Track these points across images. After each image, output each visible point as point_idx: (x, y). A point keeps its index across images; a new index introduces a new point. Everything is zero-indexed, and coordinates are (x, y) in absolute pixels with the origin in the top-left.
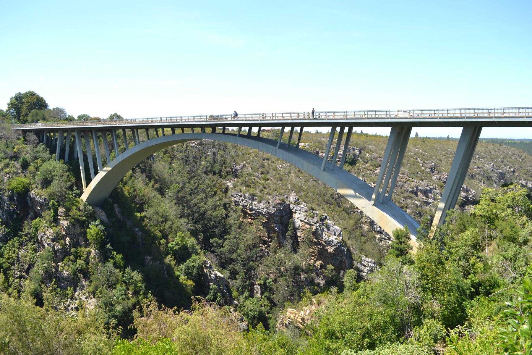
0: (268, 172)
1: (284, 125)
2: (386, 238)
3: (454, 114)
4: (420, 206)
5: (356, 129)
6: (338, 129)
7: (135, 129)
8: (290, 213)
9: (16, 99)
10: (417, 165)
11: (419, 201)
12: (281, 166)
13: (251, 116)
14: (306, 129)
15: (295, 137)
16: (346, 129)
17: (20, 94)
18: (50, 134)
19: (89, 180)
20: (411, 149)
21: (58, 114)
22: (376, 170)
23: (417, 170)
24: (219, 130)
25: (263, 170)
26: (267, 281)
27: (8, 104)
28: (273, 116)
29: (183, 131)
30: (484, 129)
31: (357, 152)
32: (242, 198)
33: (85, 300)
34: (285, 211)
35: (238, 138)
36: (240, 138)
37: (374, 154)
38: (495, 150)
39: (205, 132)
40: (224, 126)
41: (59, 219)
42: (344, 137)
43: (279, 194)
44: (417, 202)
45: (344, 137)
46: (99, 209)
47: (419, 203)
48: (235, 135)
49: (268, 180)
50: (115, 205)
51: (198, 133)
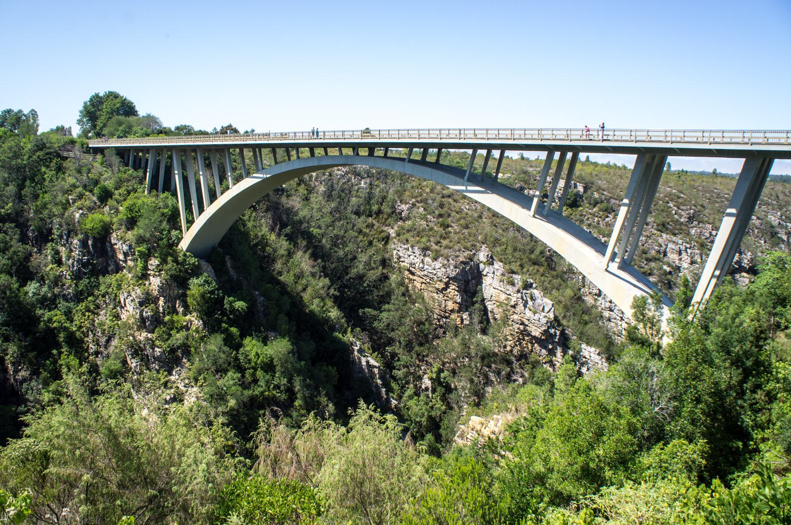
0: (449, 216)
1: (475, 147)
2: (618, 318)
3: (731, 138)
4: (670, 273)
5: (582, 156)
6: (557, 155)
7: (256, 148)
8: (478, 277)
9: (93, 105)
10: (667, 212)
11: (669, 265)
12: (467, 207)
13: (681, 134)
14: (508, 153)
15: (492, 165)
16: (569, 155)
17: (97, 96)
18: (138, 154)
19: (190, 222)
20: (663, 189)
21: (152, 126)
22: (607, 217)
23: (668, 220)
24: (379, 152)
25: (443, 211)
26: (442, 375)
27: (81, 112)
28: (460, 134)
29: (341, 151)
30: (670, 159)
31: (580, 188)
32: (409, 253)
33: (184, 389)
34: (472, 274)
35: (407, 164)
36: (411, 164)
37: (605, 193)
38: (784, 193)
39: (358, 154)
40: (386, 146)
41: (150, 275)
42: (566, 166)
43: (465, 248)
44: (665, 267)
45: (566, 166)
46: (204, 263)
47: (668, 269)
48: (403, 160)
49: (448, 226)
50: (227, 258)
51: (347, 156)
